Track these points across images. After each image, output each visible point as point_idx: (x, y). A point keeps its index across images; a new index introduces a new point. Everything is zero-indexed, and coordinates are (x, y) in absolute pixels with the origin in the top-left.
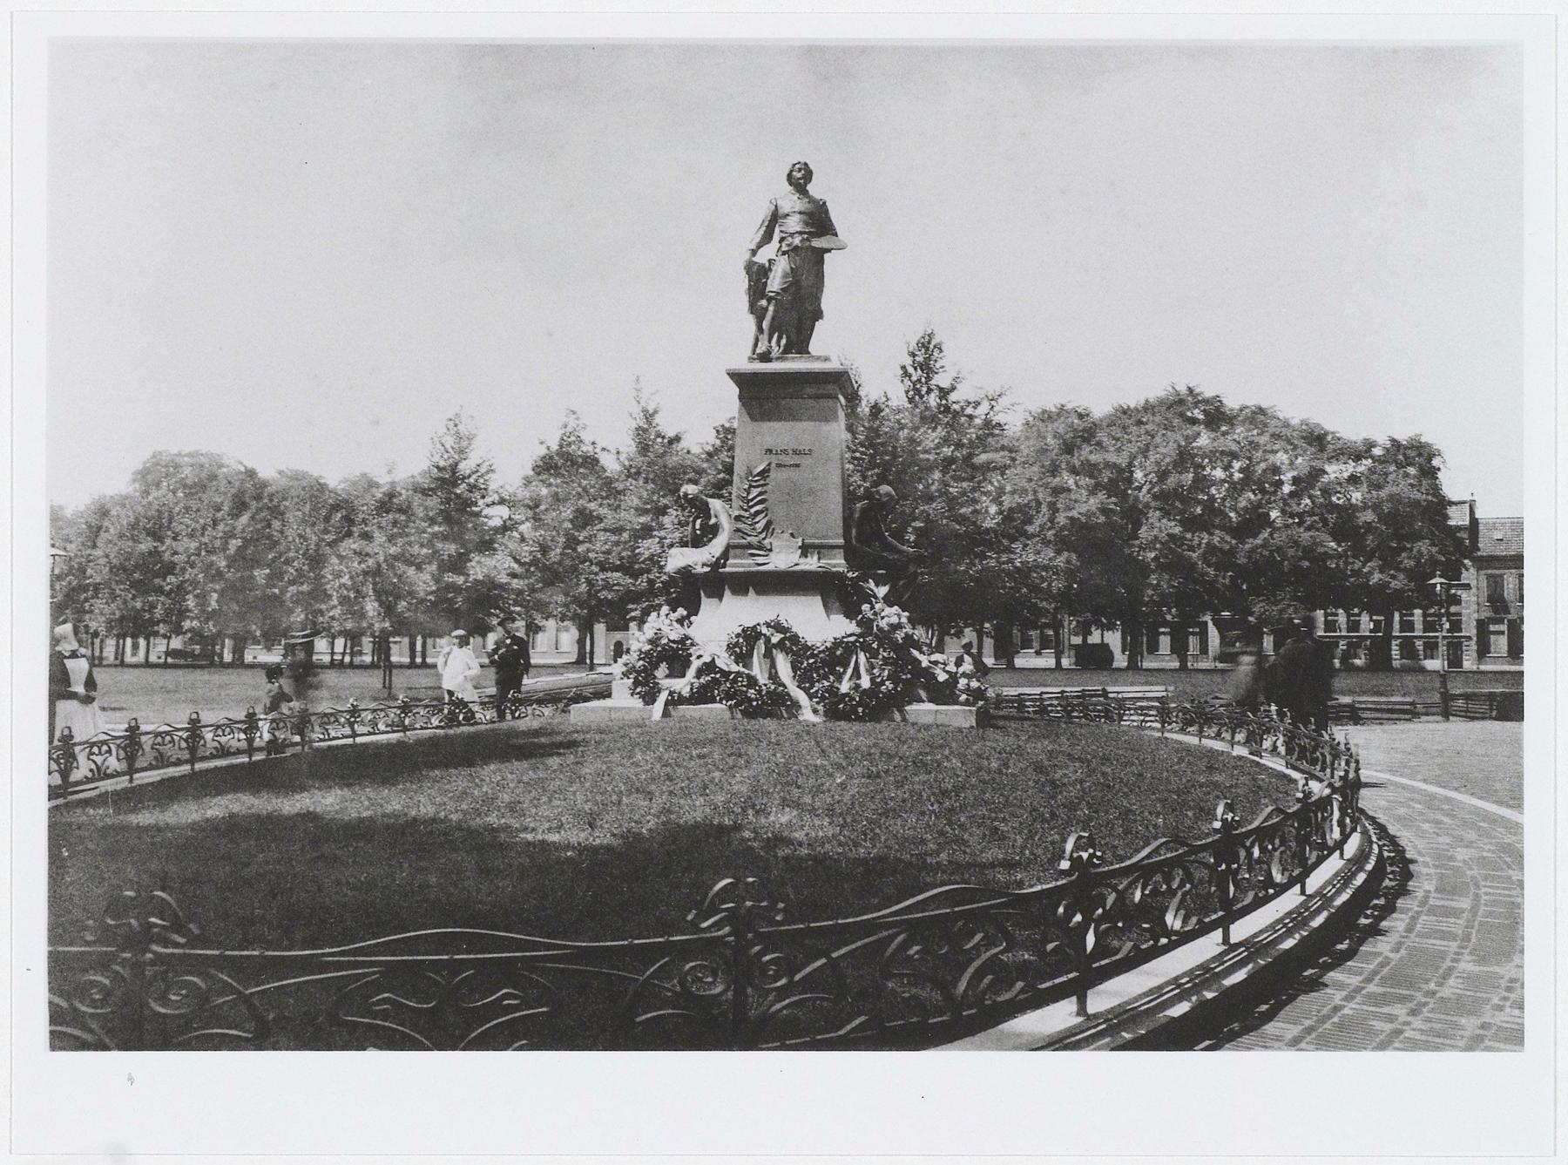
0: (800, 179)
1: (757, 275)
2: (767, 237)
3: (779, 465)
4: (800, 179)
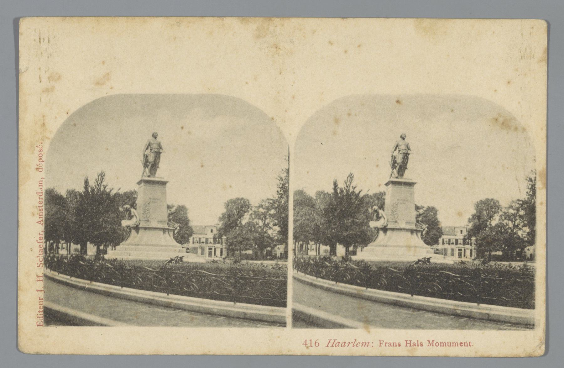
0: (155, 136)
1: (146, 157)
2: (147, 149)
4: (155, 136)
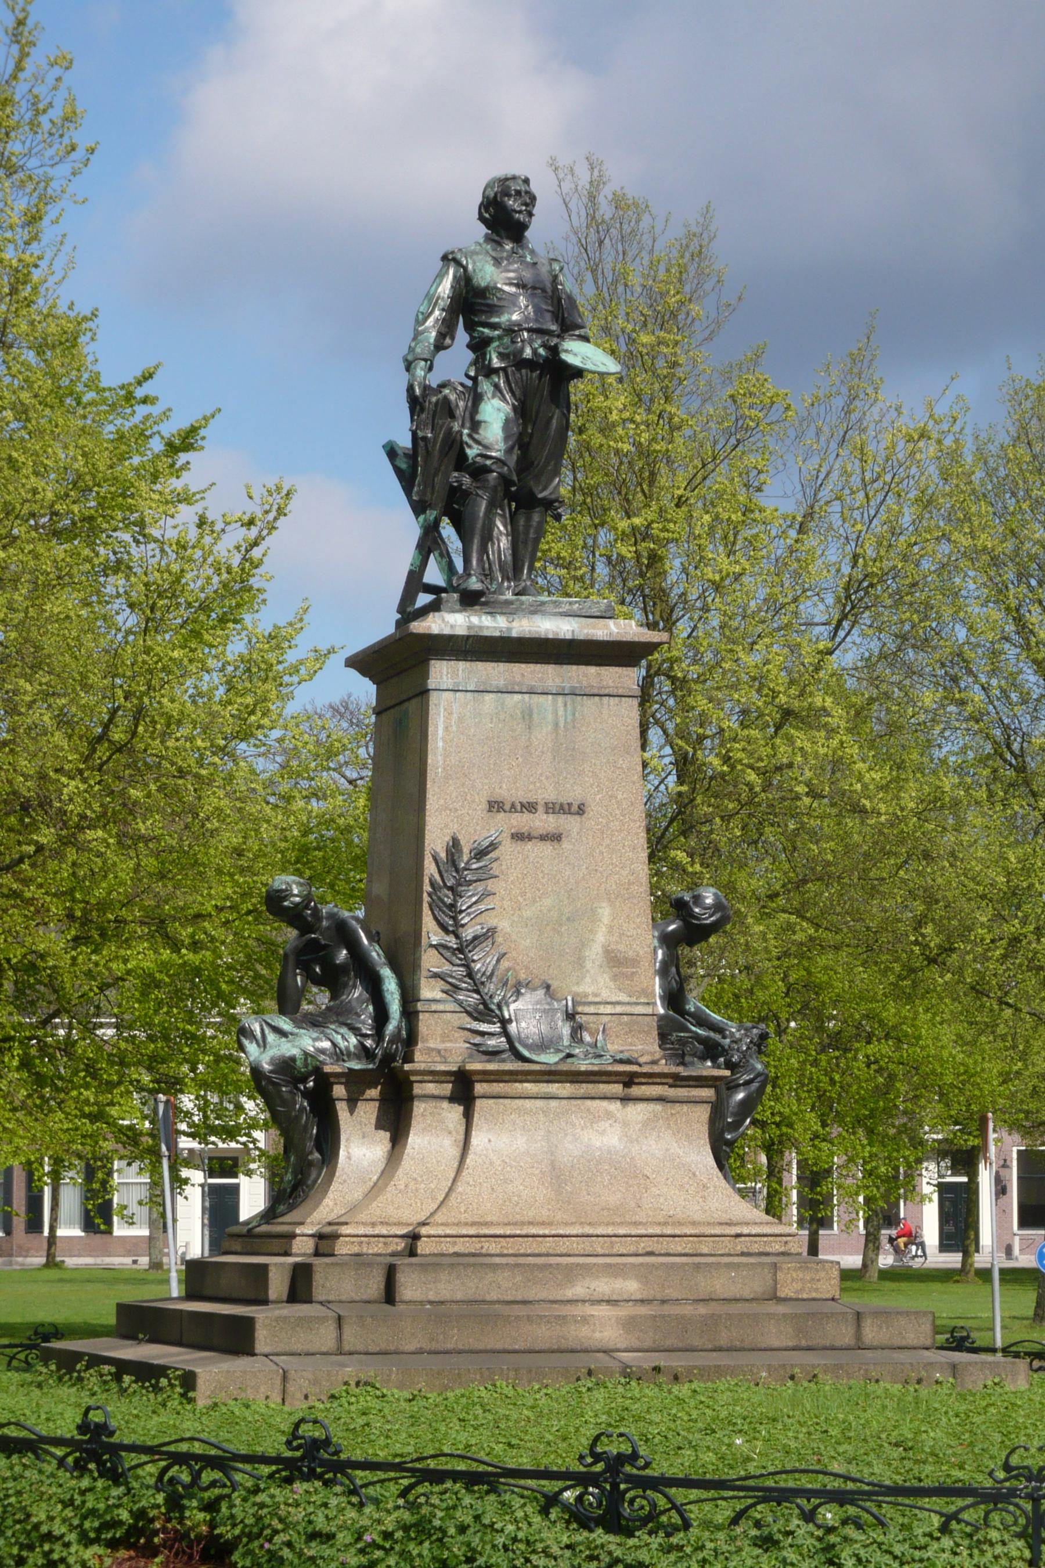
3: (519, 837)
